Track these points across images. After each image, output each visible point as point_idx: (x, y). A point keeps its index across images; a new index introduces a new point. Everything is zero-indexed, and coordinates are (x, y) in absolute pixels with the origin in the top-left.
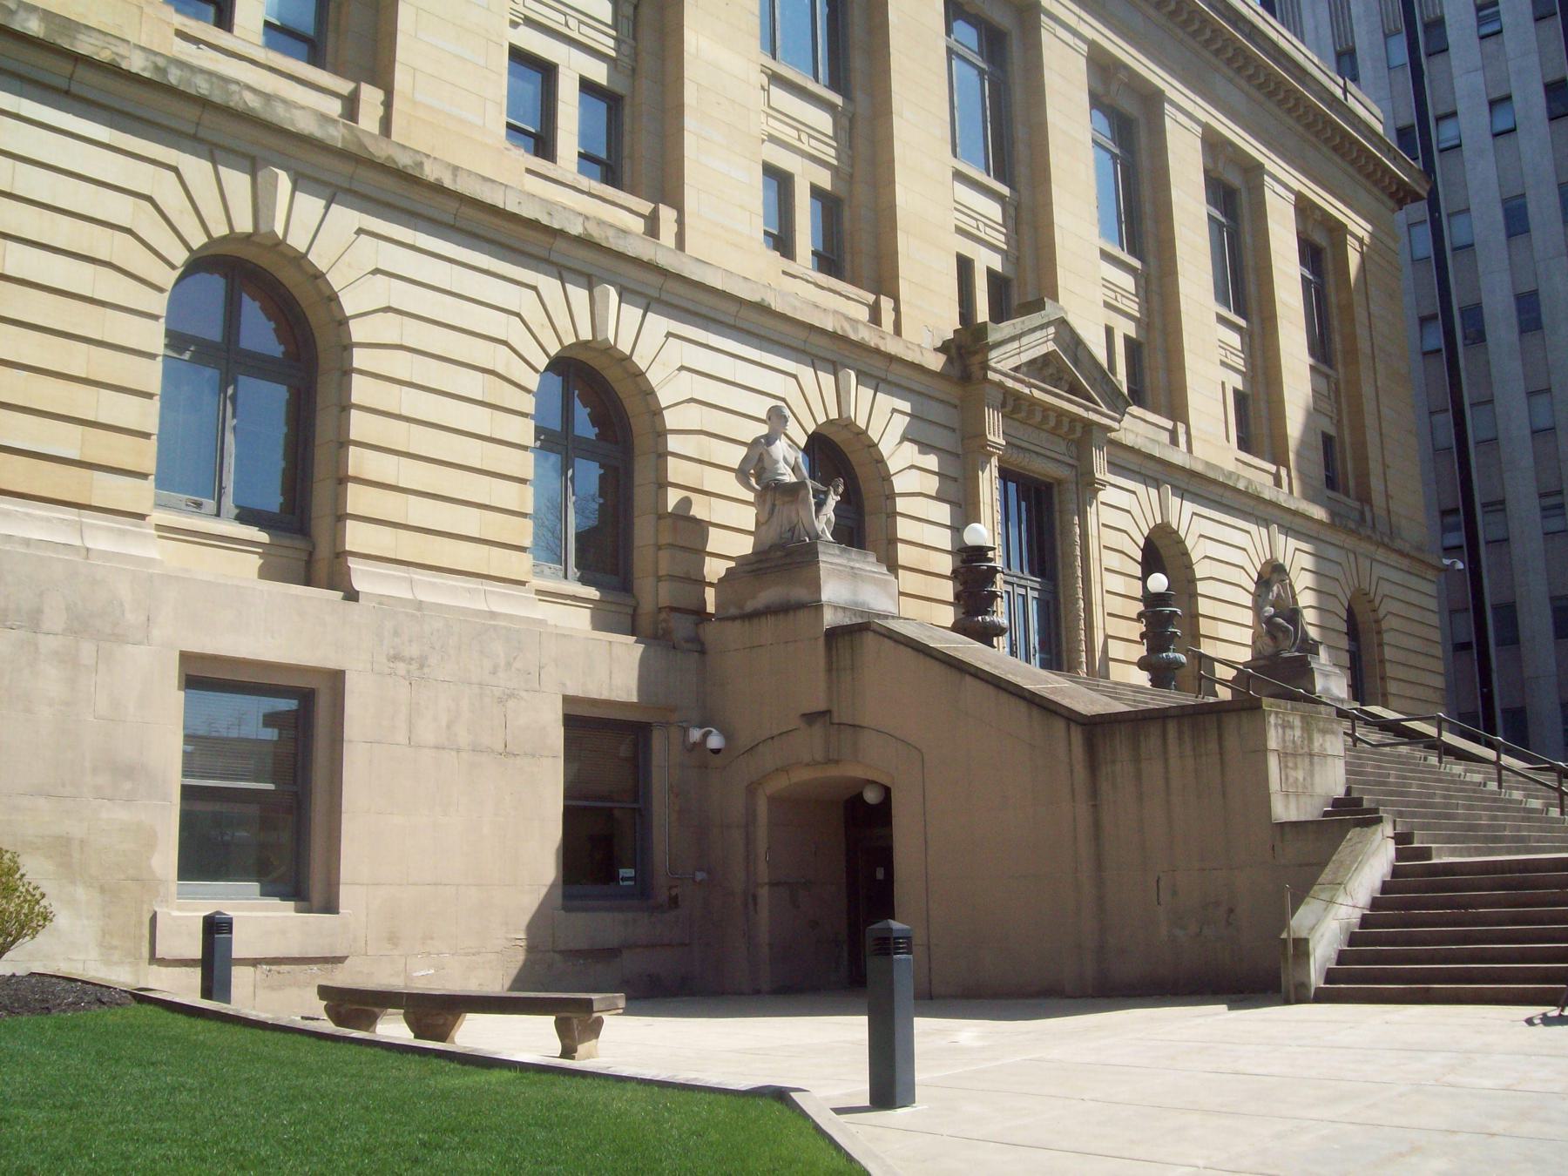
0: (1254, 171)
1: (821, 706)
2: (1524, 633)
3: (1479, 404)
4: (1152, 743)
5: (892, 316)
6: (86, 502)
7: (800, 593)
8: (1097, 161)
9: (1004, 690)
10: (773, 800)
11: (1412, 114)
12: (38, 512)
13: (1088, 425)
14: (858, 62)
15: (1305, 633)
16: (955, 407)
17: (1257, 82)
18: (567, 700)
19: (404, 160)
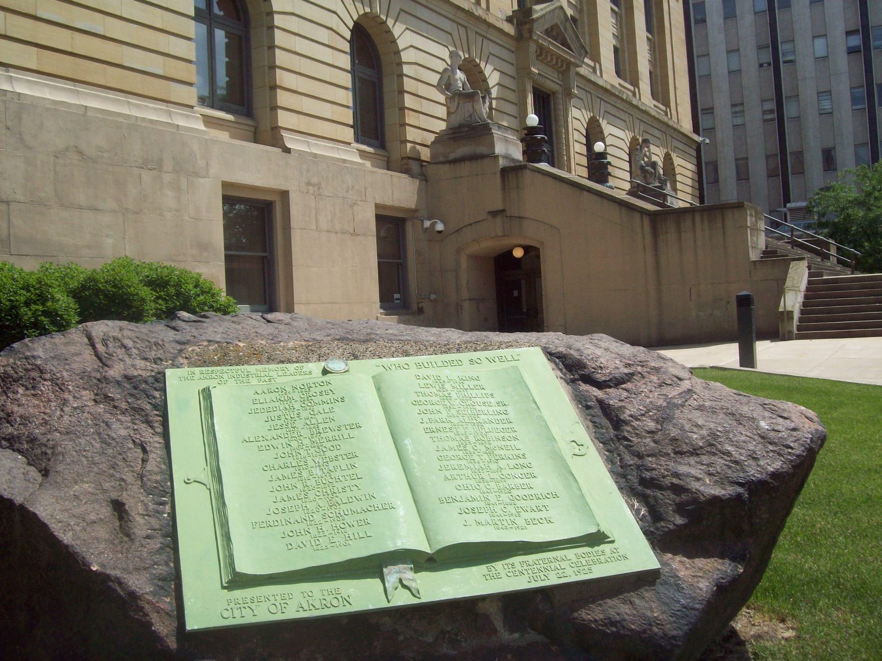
1: (500, 207)
3: (705, 56)
4: (687, 223)
6: (168, 99)
7: (482, 150)
9: (606, 198)
10: (471, 257)
12: (151, 105)
13: (569, 64)
16: (513, 52)
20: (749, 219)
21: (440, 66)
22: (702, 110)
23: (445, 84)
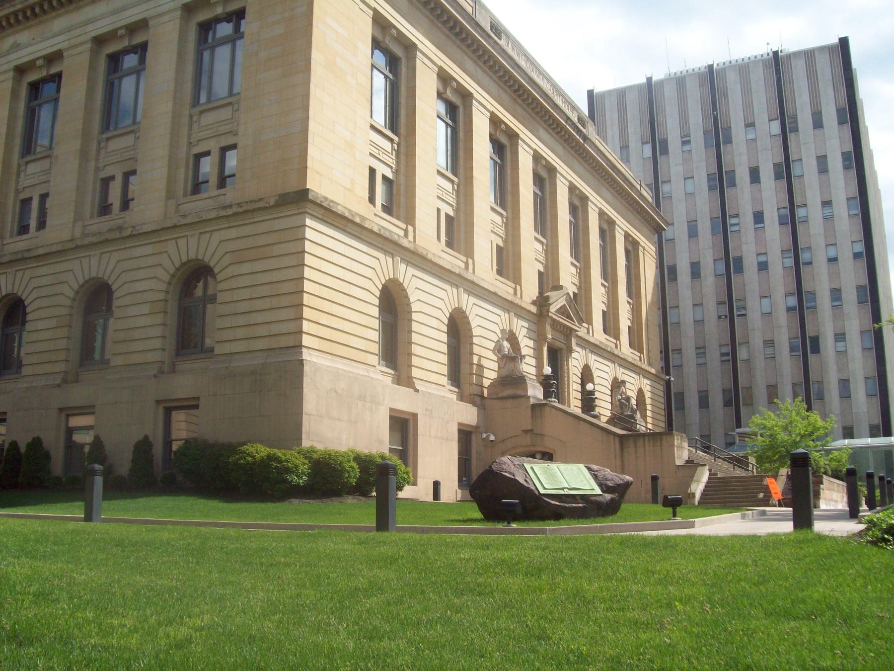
0: (514, 137)
1: (529, 427)
2: (687, 405)
4: (640, 442)
5: (472, 266)
7: (520, 392)
8: (491, 163)
13: (571, 330)
14: (509, 198)
15: (632, 406)
16: (536, 324)
17: (514, 89)
18: (459, 424)
20: (676, 441)
21: (496, 339)
22: (672, 350)
23: (498, 349)
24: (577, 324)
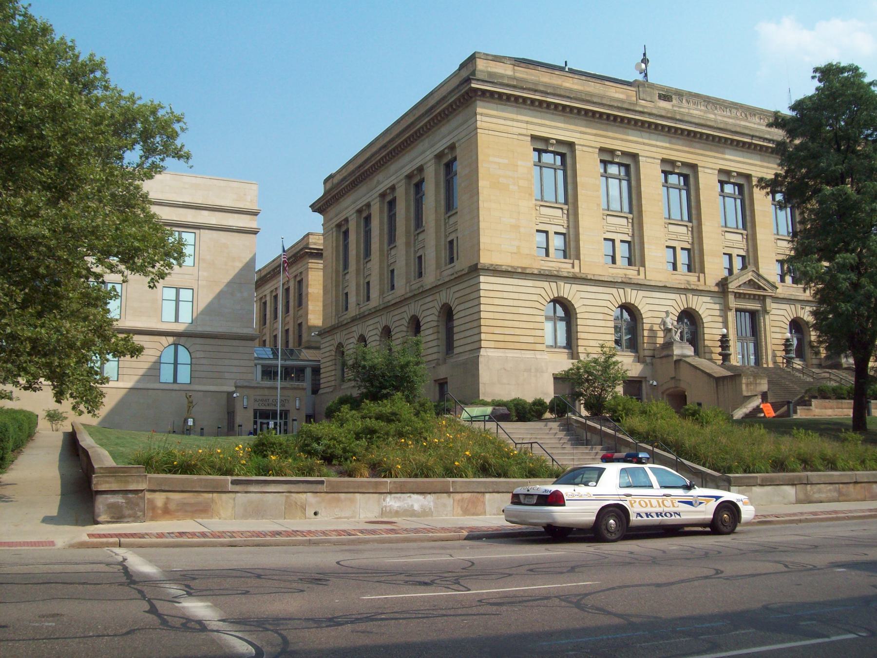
1: (673, 376)
4: (725, 382)
7: (670, 353)
11: (394, 498)
19: (584, 276)
24: (770, 291)
